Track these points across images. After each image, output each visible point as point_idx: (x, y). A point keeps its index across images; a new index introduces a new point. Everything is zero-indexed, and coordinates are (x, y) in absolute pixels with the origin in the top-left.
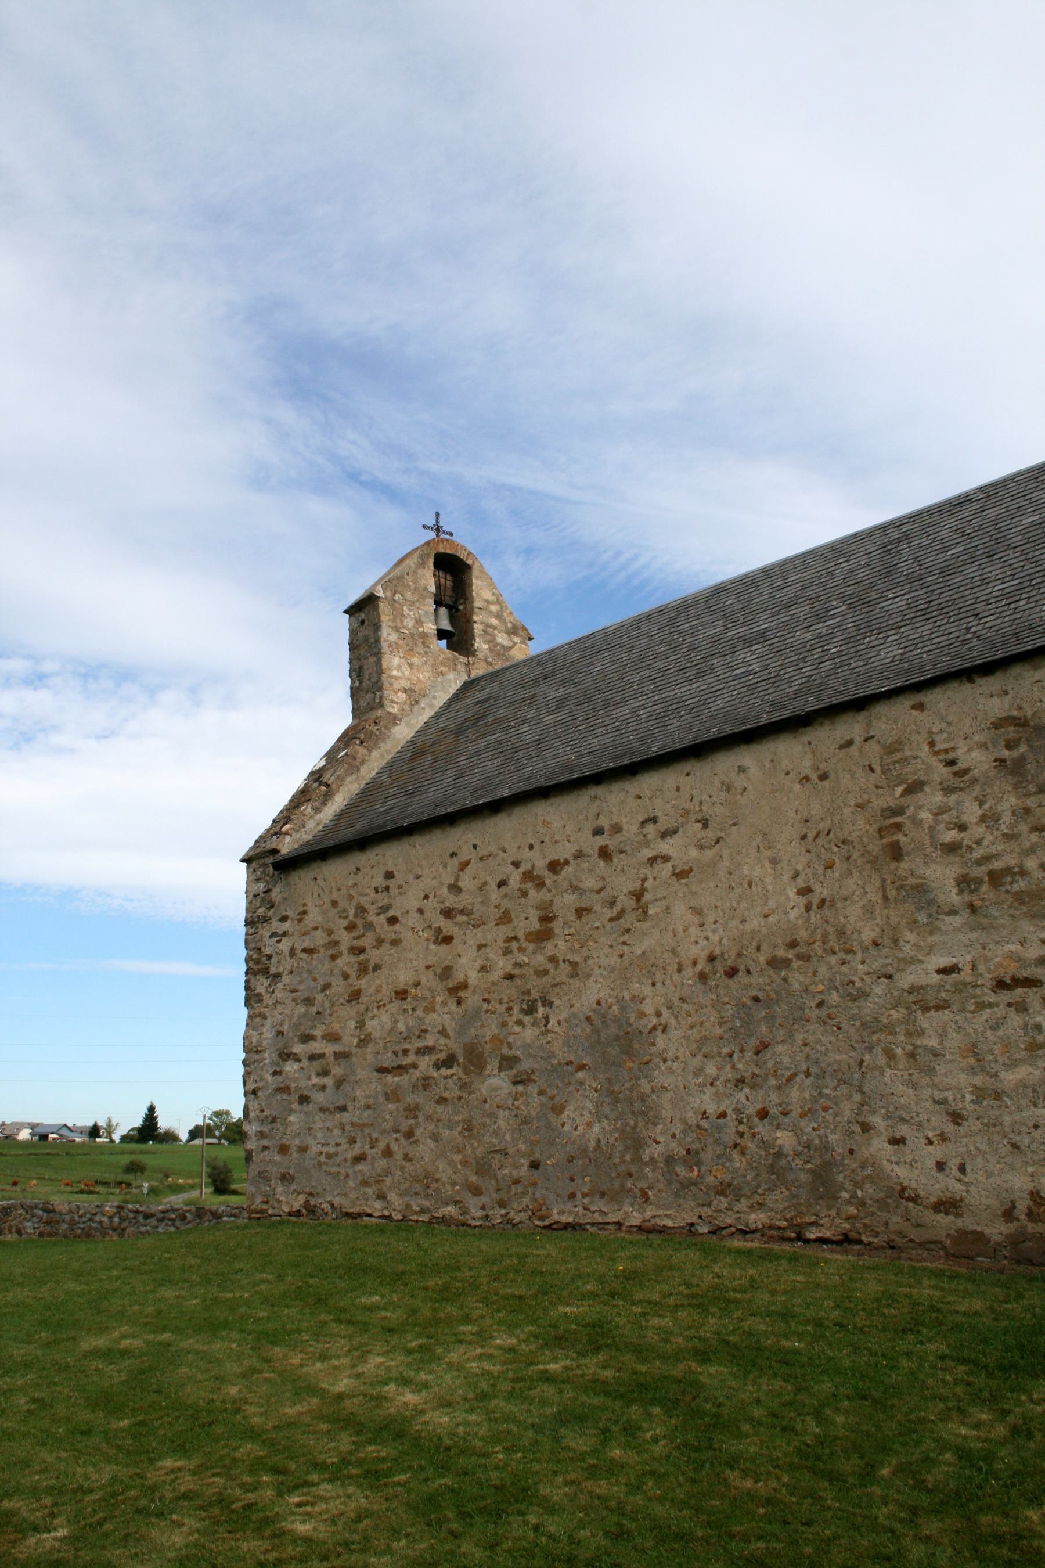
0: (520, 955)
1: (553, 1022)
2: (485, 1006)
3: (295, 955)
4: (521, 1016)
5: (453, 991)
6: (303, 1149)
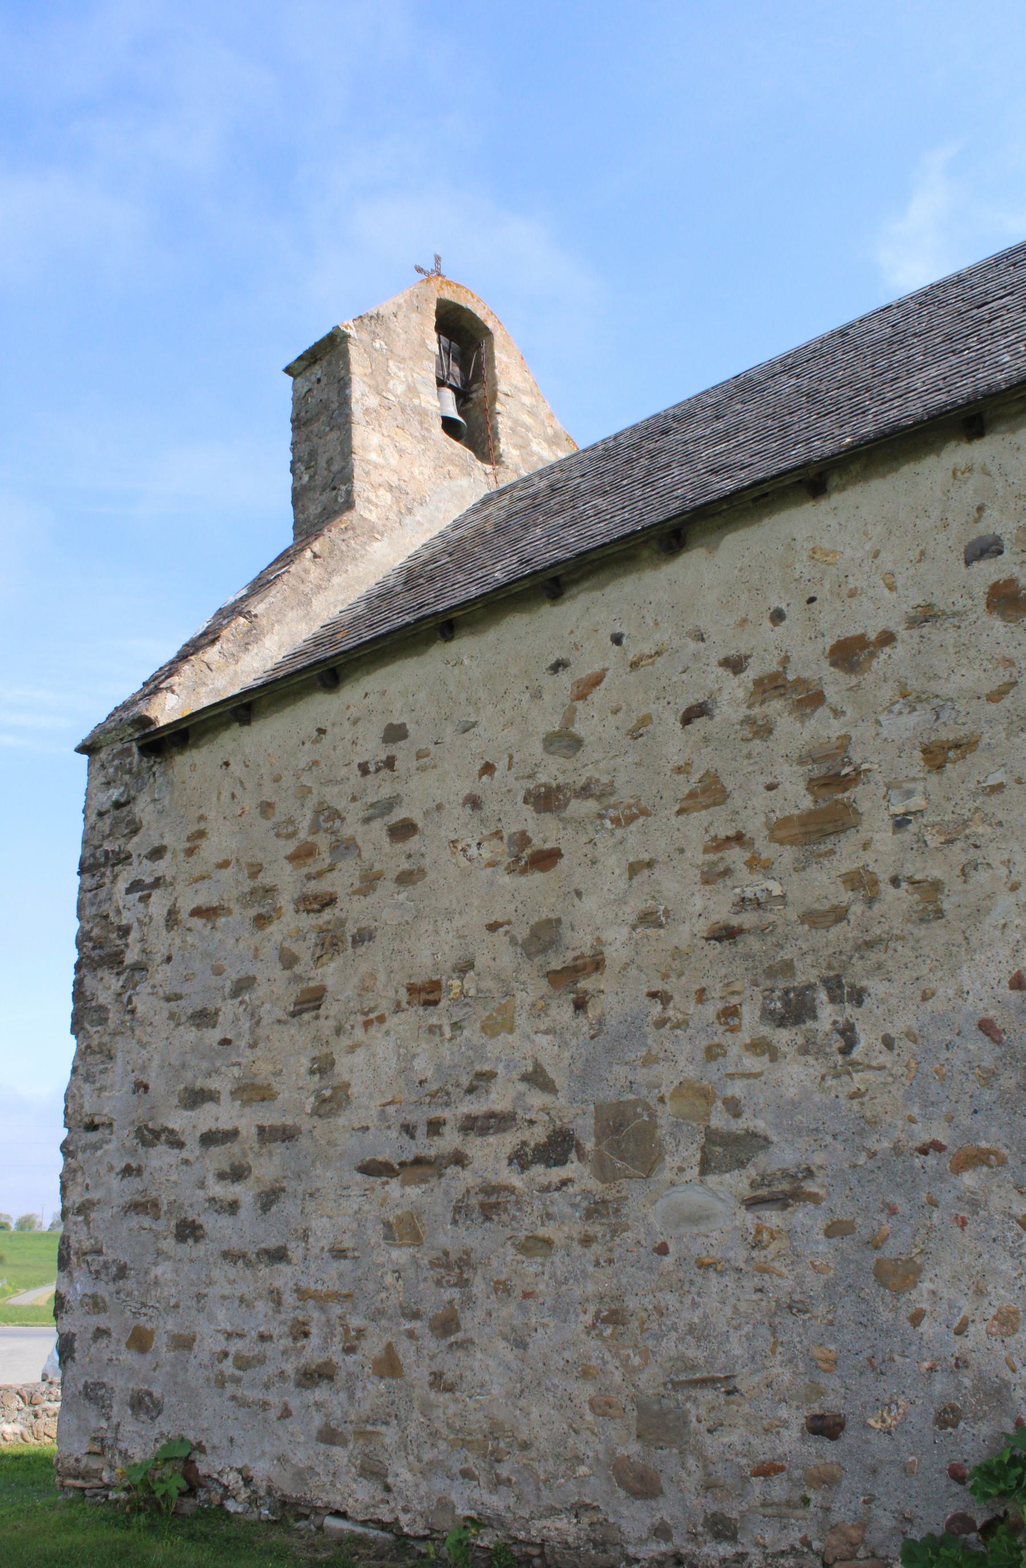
0: (757, 877)
1: (866, 1039)
2: (656, 1009)
3: (176, 922)
4: (765, 1030)
5: (560, 979)
6: (184, 1343)
